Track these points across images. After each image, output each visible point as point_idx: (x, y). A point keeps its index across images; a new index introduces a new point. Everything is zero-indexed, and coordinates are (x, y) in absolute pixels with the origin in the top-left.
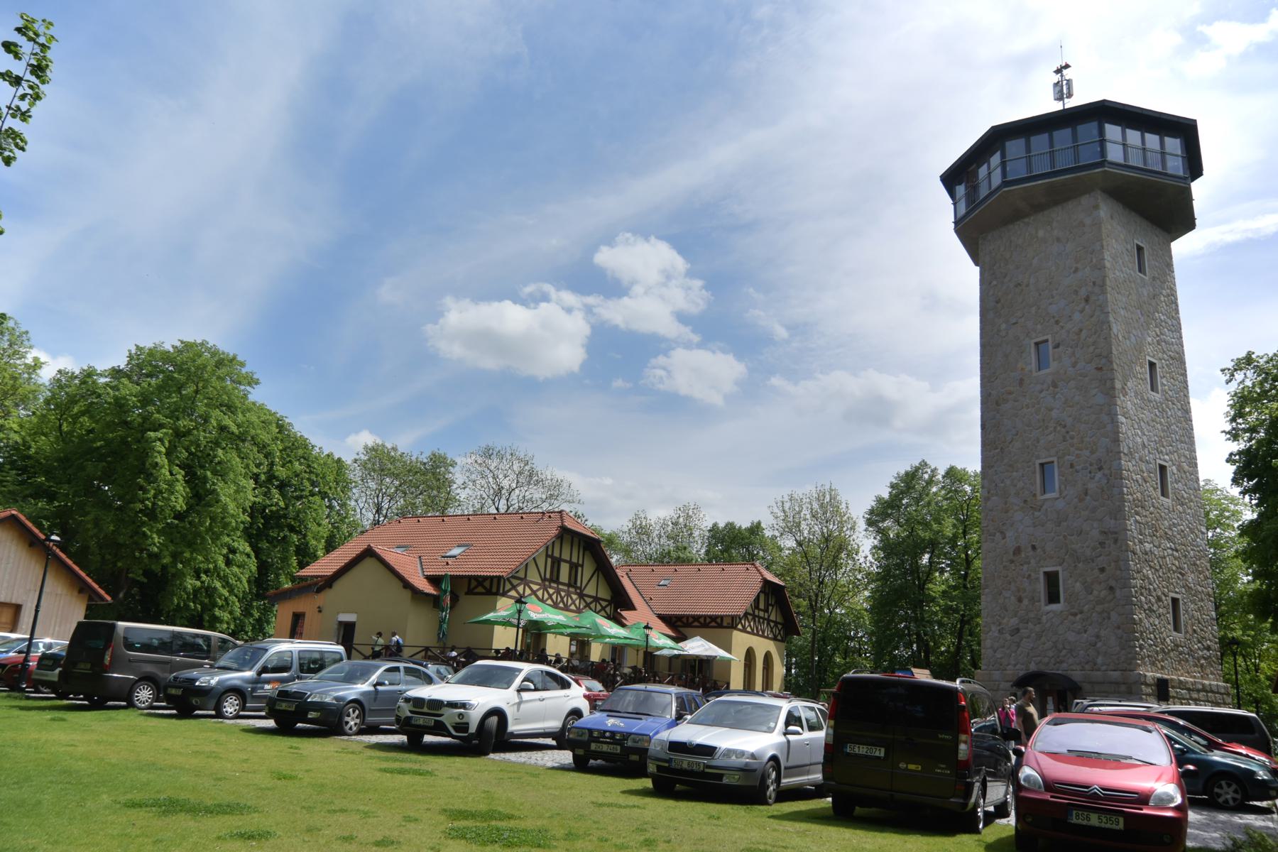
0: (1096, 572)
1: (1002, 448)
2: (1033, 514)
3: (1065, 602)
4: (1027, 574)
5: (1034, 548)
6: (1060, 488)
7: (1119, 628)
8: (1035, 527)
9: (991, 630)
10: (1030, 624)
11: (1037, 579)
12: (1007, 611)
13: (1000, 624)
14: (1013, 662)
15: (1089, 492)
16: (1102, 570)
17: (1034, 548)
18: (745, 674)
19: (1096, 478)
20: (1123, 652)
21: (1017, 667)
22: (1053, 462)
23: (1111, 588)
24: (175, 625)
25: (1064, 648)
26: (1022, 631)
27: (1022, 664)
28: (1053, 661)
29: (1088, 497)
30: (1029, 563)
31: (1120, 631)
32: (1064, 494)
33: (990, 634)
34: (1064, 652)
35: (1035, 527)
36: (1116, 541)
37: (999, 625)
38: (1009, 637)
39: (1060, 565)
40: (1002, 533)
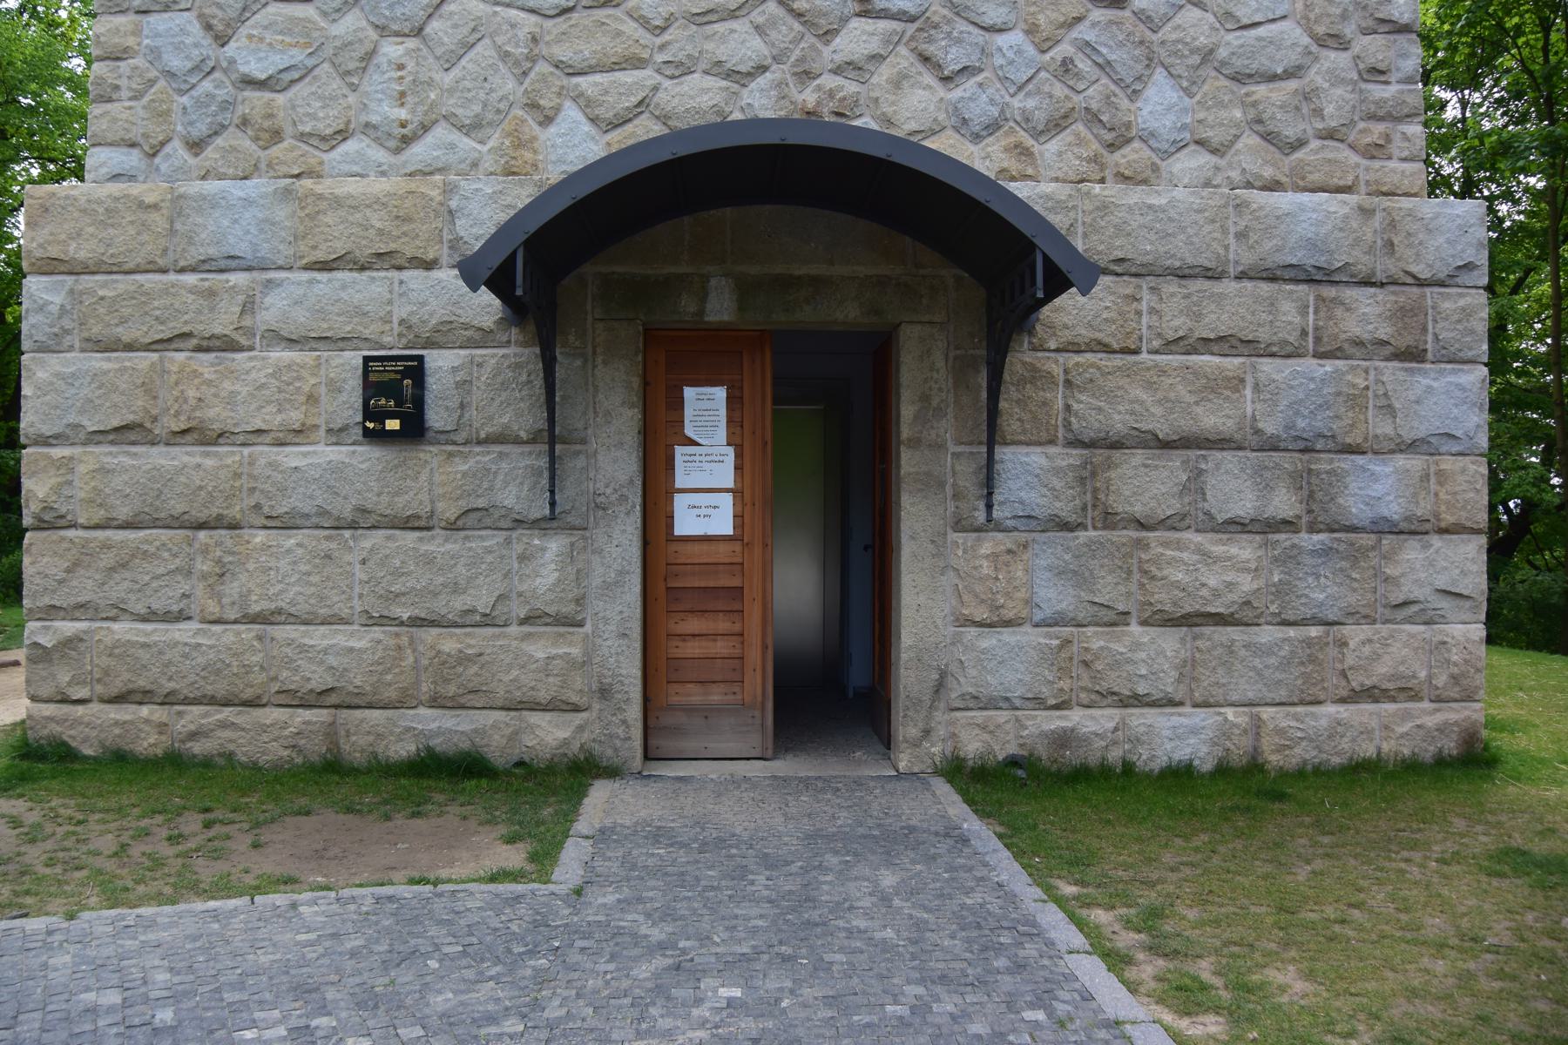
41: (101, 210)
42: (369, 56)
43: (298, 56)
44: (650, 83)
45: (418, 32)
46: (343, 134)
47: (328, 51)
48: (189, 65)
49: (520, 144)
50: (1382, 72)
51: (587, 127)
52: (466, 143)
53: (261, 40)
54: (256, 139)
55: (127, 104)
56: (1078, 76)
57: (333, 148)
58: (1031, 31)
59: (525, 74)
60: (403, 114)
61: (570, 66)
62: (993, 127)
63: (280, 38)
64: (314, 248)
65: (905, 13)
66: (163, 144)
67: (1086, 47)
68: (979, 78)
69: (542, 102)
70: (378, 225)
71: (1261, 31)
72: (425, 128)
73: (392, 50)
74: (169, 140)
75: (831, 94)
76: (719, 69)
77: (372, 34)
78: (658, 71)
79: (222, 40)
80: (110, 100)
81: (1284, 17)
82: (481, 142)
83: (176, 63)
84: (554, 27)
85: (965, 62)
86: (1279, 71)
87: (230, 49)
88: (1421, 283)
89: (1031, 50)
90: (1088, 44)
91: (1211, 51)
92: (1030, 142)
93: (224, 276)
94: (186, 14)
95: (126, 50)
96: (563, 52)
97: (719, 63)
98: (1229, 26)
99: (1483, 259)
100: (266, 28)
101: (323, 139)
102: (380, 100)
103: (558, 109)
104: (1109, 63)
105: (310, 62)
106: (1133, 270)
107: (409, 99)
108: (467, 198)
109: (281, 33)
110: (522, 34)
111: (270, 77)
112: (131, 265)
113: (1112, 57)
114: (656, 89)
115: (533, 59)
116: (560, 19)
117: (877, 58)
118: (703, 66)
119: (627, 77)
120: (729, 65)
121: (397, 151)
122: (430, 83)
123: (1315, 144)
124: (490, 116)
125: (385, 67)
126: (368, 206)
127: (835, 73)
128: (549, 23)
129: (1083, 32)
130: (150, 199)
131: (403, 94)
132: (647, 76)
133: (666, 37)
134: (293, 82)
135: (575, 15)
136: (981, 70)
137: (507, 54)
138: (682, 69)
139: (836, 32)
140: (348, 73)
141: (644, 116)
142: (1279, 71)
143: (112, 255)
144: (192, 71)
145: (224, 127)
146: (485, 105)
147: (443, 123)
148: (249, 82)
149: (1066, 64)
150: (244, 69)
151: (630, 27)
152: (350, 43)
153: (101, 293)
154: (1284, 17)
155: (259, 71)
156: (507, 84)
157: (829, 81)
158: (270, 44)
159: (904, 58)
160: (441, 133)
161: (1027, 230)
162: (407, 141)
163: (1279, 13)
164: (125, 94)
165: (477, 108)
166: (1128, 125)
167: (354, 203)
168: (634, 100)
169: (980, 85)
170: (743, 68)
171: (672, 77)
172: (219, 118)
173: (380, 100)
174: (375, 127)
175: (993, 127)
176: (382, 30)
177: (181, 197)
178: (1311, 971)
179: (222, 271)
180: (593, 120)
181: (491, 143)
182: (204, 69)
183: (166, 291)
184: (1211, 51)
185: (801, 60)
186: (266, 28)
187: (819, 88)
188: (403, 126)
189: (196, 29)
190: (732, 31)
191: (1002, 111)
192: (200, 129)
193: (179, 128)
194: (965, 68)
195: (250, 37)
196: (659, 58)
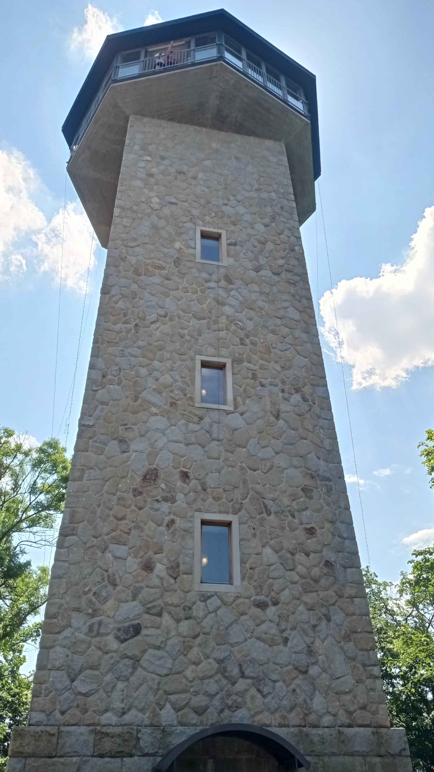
0: (300, 533)
1: (136, 325)
2: (187, 425)
3: (243, 579)
4: (167, 519)
5: (185, 476)
6: (235, 399)
7: (347, 638)
8: (187, 445)
9: (69, 626)
10: (166, 616)
11: (188, 532)
12: (115, 585)
13: (95, 613)
14: (118, 705)
15: (282, 415)
16: (311, 532)
17: (185, 476)
18: (294, 61)
19: (292, 400)
20: (361, 686)
21: (127, 718)
22: (231, 583)
23: (328, 564)
24: (124, 84)
25: (243, 676)
26: (144, 632)
27: (142, 710)
28: (216, 702)
29: (281, 423)
30: (173, 500)
31: (350, 647)
32: (241, 409)
33: (66, 633)
34: (241, 684)
35: (187, 445)
36: (329, 490)
37: (92, 616)
38: (114, 645)
39: (235, 512)
40: (122, 441)
41: (37, 736)
42: (114, 686)
43: (94, 686)
44: (189, 697)
45: (127, 680)
46: (106, 711)
47: (103, 685)
48: (63, 687)
49: (154, 716)
50: (373, 689)
51: (172, 711)
52: (140, 715)
53: (85, 681)
54: (81, 712)
55: (44, 698)
56: (297, 694)
57: (102, 715)
58: (284, 681)
59: (156, 694)
60: (123, 705)
61: (168, 692)
62: (276, 710)
63: (90, 680)
64: (100, 749)
65: (253, 677)
66: (53, 712)
67: (298, 686)
68: (272, 695)
69: (161, 703)
70: (119, 742)
71: (342, 679)
72: (129, 710)
73: (120, 685)
74: (55, 710)
75: (235, 701)
76: (206, 694)
77: (115, 680)
78: (191, 694)
79: (73, 681)
80: (38, 697)
81: (347, 674)
82: (144, 715)
83: (59, 686)
84: (164, 679)
85: (268, 691)
86: (347, 690)
87: (75, 683)
88: (392, 756)
89: (284, 687)
90: (299, 684)
91: (330, 686)
92: (286, 714)
93: (71, 759)
94: (63, 671)
95: (45, 681)
96: (167, 688)
97: (207, 692)
98: (333, 678)
99: (407, 746)
100: (86, 677)
101: (100, 712)
102: (117, 701)
103: (165, 705)
104: (304, 690)
105: (98, 688)
106: (316, 754)
107: (125, 701)
108: (143, 734)
109: (90, 679)
110: (156, 681)
111: (86, 693)
112: (43, 755)
113: (305, 689)
114: (190, 699)
115: (158, 689)
116: (165, 677)
117: (246, 690)
118: (202, 692)
119: (183, 696)
120: (209, 693)
121: (121, 717)
122: (131, 696)
123: (359, 711)
124: (147, 707)
125: (118, 691)
126: (116, 736)
127: (236, 695)
128: (163, 678)
129: (297, 681)
130: (52, 732)
131: (123, 699)
132: (187, 695)
133: (193, 684)
134: (92, 694)
135: (170, 676)
136: (272, 693)
137: (152, 688)
138: (196, 693)
139: (236, 682)
140: (108, 692)
141: (187, 707)
142: (347, 690)
143: (39, 751)
144: (63, 689)
145: (71, 707)
146: (145, 703)
147: (134, 708)
148: (80, 693)
149: (294, 690)
150: (79, 689)
151: (184, 681)
152: (109, 683)
153: (33, 764)
154: (347, 674)
155: (83, 690)
156: (151, 698)
157: (234, 697)
158: (87, 682)
159: (253, 691)
160: (133, 712)
161: (292, 752)
162: (124, 713)
163: (346, 674)
164: (43, 695)
165: (143, 704)
166: (310, 708)
167: (112, 735)
168: (185, 702)
169: (273, 698)
170: (213, 693)
171: (195, 696)
172: (71, 705)
173: (117, 701)
174: (115, 709)
175: (276, 710)
176: (118, 679)
177: (62, 731)
178: (226, 188)
179: (71, 756)
180: (174, 709)
181: (147, 715)
182: (66, 689)
183: (54, 764)
184: (330, 686)
185: (227, 691)
186: (86, 677)
187: (232, 699)
188: (123, 709)
189: (65, 676)
190: (210, 682)
191: (278, 706)
192: (65, 708)
193: (58, 706)
194: (269, 693)
195: (81, 680)
196: (192, 690)
